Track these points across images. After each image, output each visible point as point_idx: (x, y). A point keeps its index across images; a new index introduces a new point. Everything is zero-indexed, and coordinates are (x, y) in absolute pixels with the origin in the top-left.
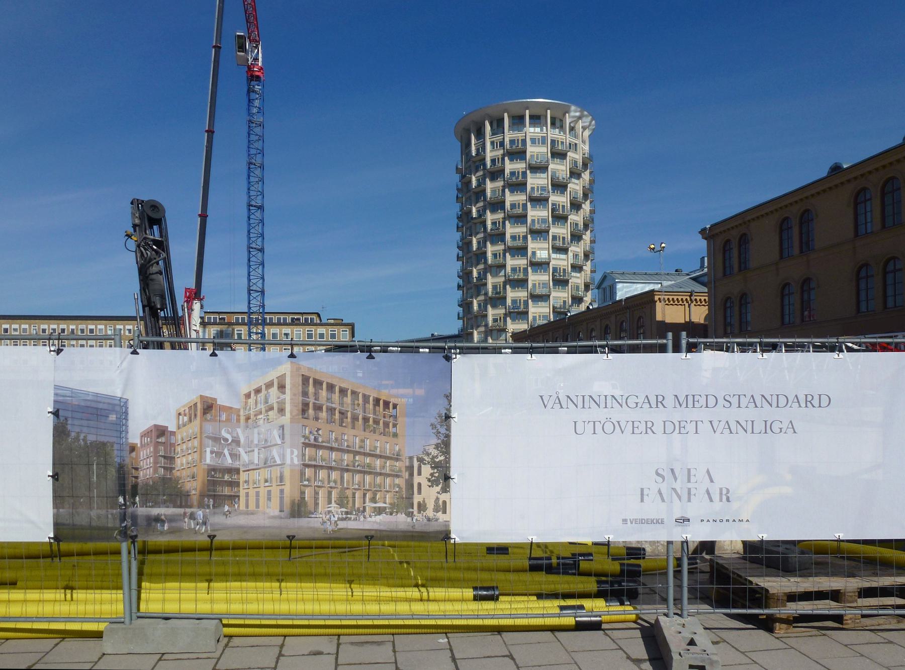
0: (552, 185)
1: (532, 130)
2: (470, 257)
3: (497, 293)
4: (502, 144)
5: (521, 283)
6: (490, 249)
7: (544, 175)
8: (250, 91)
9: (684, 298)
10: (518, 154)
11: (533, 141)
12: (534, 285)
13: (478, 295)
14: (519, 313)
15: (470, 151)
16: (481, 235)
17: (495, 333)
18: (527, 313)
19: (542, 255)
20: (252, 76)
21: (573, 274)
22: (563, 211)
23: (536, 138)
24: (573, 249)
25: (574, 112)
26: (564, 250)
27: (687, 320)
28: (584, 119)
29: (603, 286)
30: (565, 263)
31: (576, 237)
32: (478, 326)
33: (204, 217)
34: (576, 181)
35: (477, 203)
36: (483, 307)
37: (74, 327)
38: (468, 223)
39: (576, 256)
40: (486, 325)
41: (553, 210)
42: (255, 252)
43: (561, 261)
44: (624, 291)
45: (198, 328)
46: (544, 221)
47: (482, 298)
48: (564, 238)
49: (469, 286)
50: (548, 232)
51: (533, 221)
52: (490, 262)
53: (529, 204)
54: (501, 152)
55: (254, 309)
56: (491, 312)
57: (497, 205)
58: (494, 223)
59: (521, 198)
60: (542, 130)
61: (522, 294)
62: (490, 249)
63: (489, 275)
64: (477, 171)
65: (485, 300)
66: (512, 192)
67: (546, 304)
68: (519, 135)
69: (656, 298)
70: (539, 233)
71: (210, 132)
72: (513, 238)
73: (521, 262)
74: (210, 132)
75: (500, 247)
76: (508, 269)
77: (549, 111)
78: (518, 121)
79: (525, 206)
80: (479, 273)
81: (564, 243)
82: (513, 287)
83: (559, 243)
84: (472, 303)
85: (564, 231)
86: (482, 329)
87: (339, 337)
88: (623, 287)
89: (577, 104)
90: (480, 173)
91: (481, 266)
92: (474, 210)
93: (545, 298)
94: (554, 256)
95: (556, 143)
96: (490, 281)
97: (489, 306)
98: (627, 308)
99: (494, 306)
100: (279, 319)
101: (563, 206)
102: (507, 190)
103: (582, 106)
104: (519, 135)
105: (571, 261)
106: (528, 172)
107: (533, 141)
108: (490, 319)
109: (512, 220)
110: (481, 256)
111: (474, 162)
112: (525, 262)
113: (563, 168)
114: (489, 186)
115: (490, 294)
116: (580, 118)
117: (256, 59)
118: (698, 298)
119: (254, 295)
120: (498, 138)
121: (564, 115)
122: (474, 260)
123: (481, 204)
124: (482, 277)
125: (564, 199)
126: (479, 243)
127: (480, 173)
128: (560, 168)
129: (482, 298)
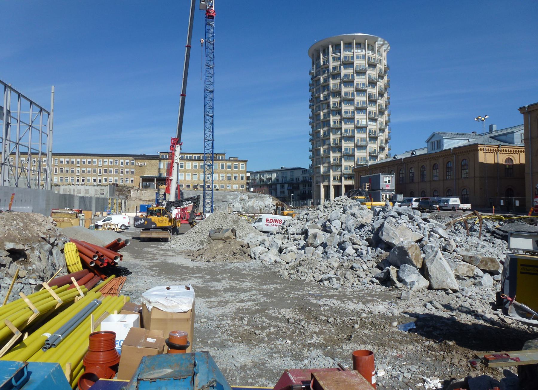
0: (369, 83)
1: (356, 51)
2: (316, 122)
3: (336, 144)
4: (339, 59)
5: (351, 138)
6: (332, 119)
7: (364, 77)
8: (207, 24)
9: (495, 149)
10: (350, 64)
11: (358, 57)
12: (358, 140)
13: (324, 144)
14: (350, 156)
15: (320, 62)
16: (326, 111)
17: (334, 167)
18: (354, 156)
19: (363, 122)
20: (209, 16)
21: (380, 134)
22: (375, 97)
23: (359, 56)
24: (379, 119)
25: (380, 41)
26: (375, 120)
27: (496, 162)
28: (385, 46)
29: (432, 140)
30: (376, 127)
31: (381, 113)
32: (324, 163)
33: (184, 96)
34: (381, 81)
35: (323, 92)
36: (327, 152)
37: (79, 160)
38: (316, 104)
39: (381, 123)
40: (329, 163)
41: (369, 97)
42: (209, 117)
43: (373, 126)
44: (449, 144)
45: (178, 161)
46: (364, 103)
47: (326, 147)
48: (375, 113)
49: (317, 140)
50: (366, 109)
51: (358, 103)
52: (332, 126)
53: (355, 93)
54: (339, 63)
55: (208, 151)
56: (332, 155)
57: (337, 93)
58: (334, 104)
59: (350, 89)
60: (362, 51)
61: (351, 145)
62: (332, 118)
63: (331, 133)
64: (324, 73)
65: (329, 148)
66: (345, 86)
67: (365, 151)
68: (350, 54)
69: (479, 148)
70: (361, 110)
71: (189, 47)
72: (346, 112)
73: (351, 126)
74: (189, 47)
75: (338, 118)
76: (343, 130)
77: (367, 41)
78: (348, 46)
79: (353, 94)
80: (324, 133)
81: (375, 116)
82: (346, 141)
83: (373, 116)
84: (320, 149)
85: (375, 109)
86: (326, 165)
87: (239, 169)
88: (447, 142)
89: (381, 37)
90: (326, 75)
91: (326, 128)
92: (322, 96)
93: (364, 147)
94: (369, 123)
95: (368, 58)
96: (332, 137)
97: (331, 152)
98: (454, 154)
99: (334, 152)
100: (187, 157)
101: (375, 95)
102: (342, 85)
103: (385, 38)
104: (350, 54)
105: (379, 126)
106: (355, 75)
107: (358, 57)
108: (331, 159)
109: (346, 102)
110: (326, 122)
111: (322, 69)
112: (353, 126)
113: (374, 73)
114: (332, 82)
115: (332, 144)
116: (382, 45)
117: (211, 6)
118: (502, 149)
119: (208, 142)
120: (337, 55)
121: (375, 43)
122: (321, 125)
123: (326, 93)
124: (327, 135)
125: (375, 91)
126: (324, 115)
127: (326, 75)
128: (372, 73)
129: (326, 147)
